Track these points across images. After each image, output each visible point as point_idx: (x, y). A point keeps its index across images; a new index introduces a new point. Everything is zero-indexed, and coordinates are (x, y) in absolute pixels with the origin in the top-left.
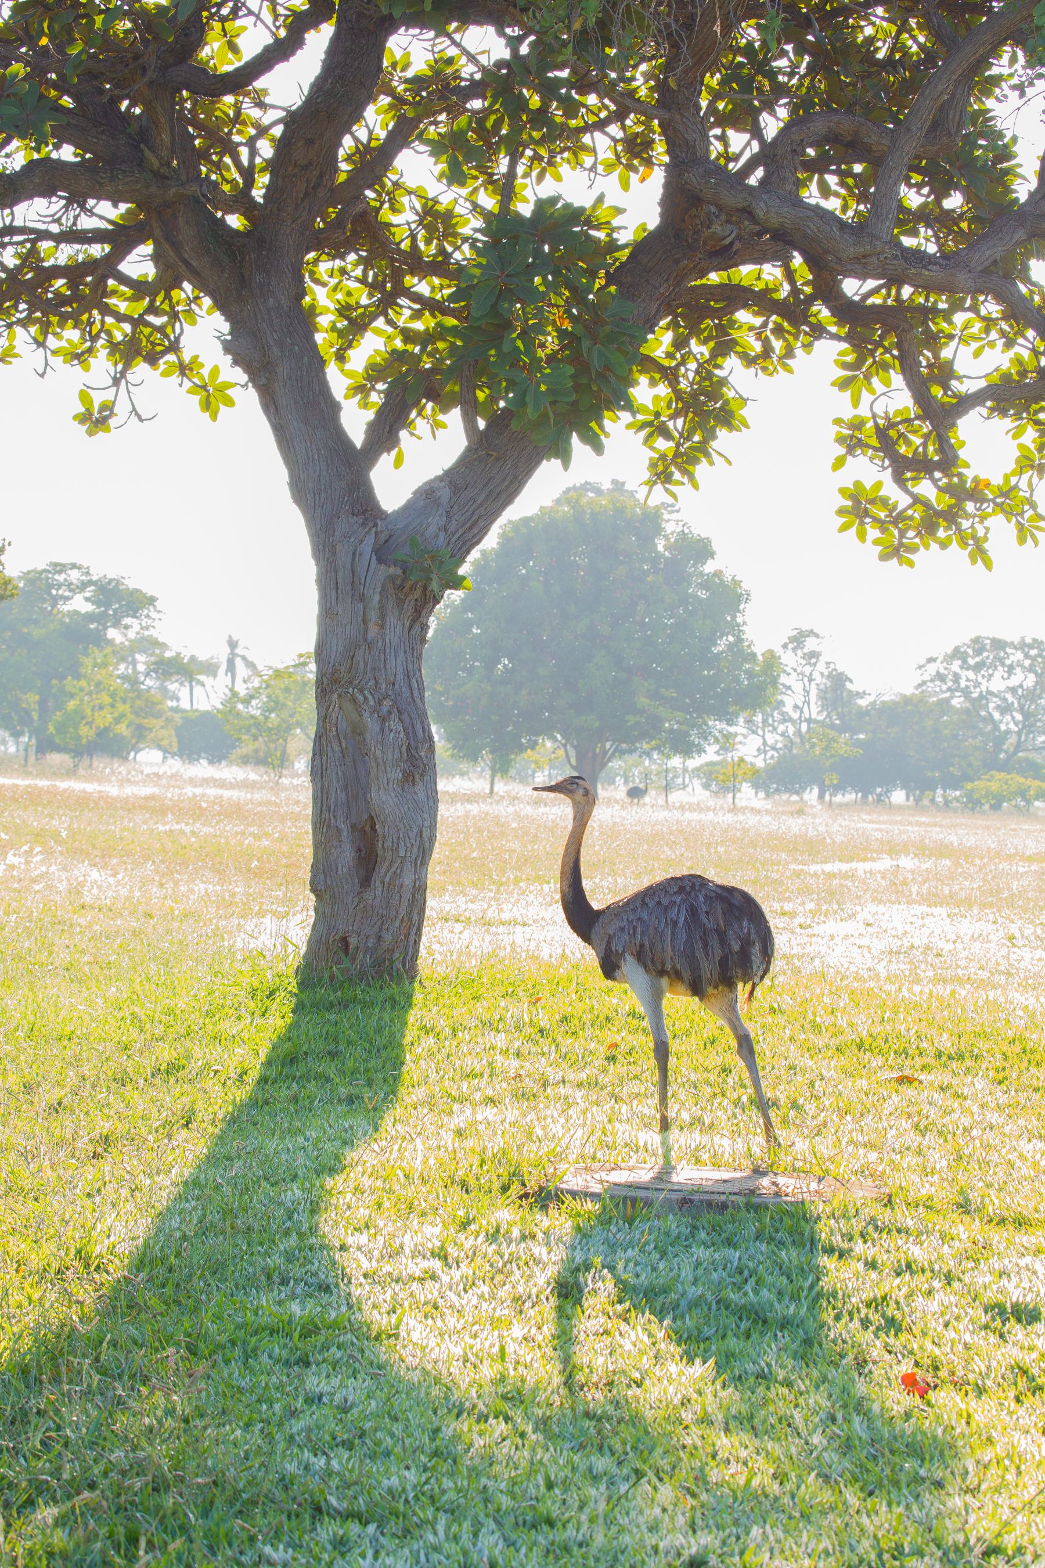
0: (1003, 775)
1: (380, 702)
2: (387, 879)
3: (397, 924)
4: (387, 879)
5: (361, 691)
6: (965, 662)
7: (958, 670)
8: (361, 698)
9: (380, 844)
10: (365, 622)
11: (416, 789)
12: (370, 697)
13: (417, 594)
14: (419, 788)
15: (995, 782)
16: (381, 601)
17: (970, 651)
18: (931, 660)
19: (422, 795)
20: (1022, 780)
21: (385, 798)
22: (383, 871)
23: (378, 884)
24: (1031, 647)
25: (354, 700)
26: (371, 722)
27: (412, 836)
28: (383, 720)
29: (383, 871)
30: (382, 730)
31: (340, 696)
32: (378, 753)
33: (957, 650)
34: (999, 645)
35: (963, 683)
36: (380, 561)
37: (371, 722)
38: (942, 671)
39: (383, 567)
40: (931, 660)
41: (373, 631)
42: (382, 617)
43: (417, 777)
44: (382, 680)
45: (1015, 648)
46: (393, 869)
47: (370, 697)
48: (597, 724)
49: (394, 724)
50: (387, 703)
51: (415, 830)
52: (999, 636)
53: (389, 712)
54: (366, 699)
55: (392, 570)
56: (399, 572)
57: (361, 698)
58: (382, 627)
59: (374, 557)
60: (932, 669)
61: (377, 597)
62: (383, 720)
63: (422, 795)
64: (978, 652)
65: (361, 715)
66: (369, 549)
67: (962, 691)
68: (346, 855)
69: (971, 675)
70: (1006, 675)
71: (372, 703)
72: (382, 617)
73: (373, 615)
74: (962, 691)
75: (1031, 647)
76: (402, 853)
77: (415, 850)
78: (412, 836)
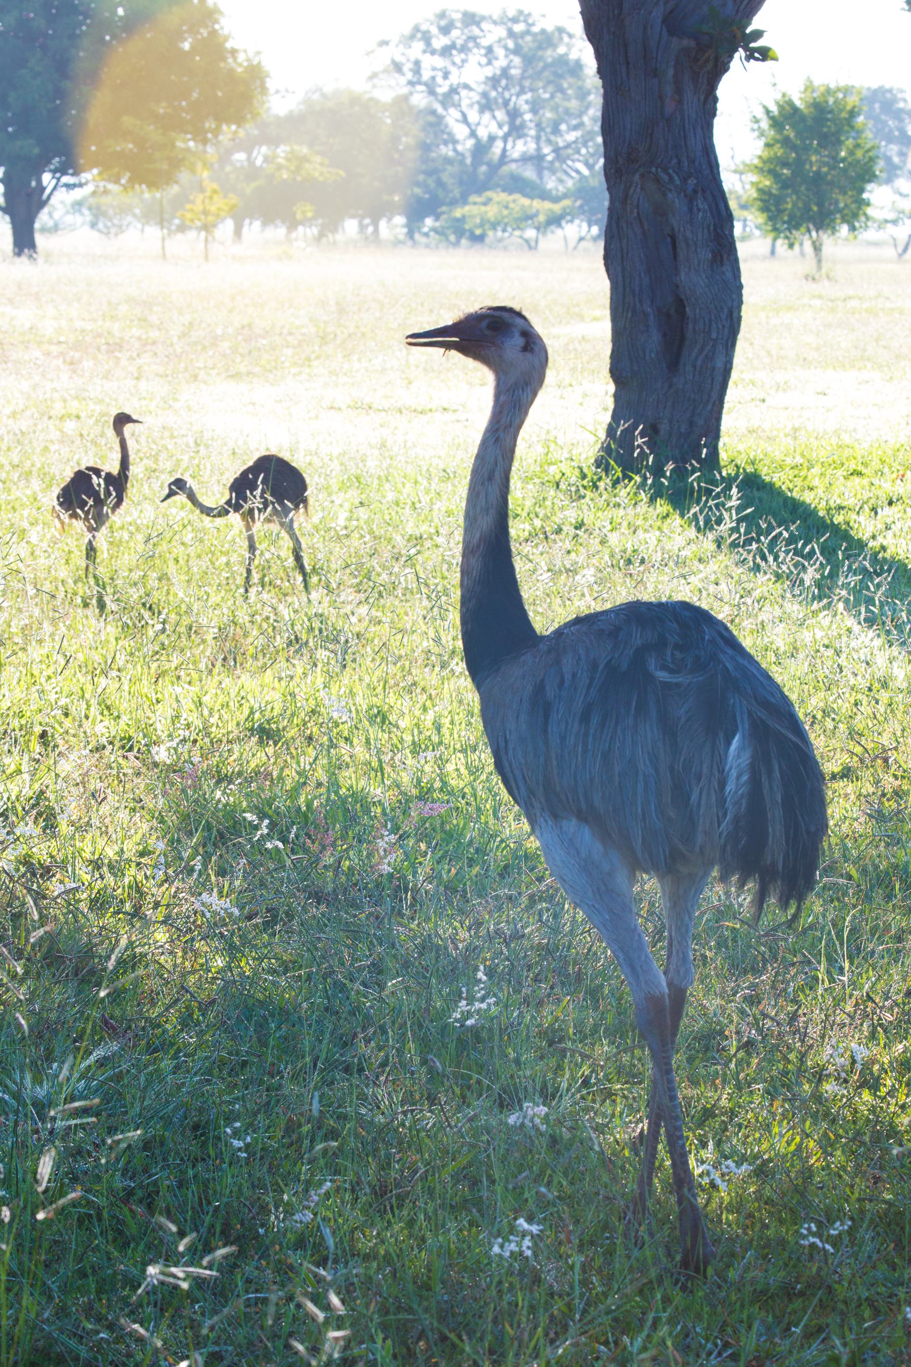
0: (503, 197)
1: (684, 180)
2: (699, 363)
3: (709, 408)
4: (699, 363)
5: (665, 170)
6: (428, 43)
7: (420, 57)
8: (665, 177)
9: (690, 326)
10: (660, 98)
11: (724, 268)
12: (675, 177)
13: (710, 66)
14: (727, 268)
15: (495, 204)
16: (675, 75)
17: (434, 30)
18: (384, 43)
19: (729, 275)
20: (526, 202)
21: (693, 279)
22: (694, 354)
23: (689, 368)
24: (515, 20)
25: (658, 180)
26: (678, 203)
27: (723, 316)
28: (691, 200)
29: (694, 354)
30: (690, 210)
31: (642, 176)
32: (688, 233)
33: (417, 29)
34: (471, 19)
35: (426, 75)
36: (671, 33)
37: (678, 203)
38: (399, 58)
39: (675, 40)
40: (384, 43)
41: (670, 106)
42: (679, 91)
43: (725, 257)
44: (684, 159)
45: (495, 23)
46: (705, 353)
47: (675, 177)
48: (36, 151)
49: (701, 203)
50: (692, 182)
51: (726, 311)
52: (471, 9)
53: (695, 192)
54: (671, 179)
55: (685, 42)
56: (693, 44)
57: (665, 177)
58: (680, 102)
59: (664, 29)
60: (383, 58)
61: (671, 72)
62: (691, 200)
63: (729, 275)
64: (445, 30)
65: (664, 195)
66: (659, 21)
67: (426, 84)
68: (653, 340)
69: (439, 61)
70: (484, 61)
71: (678, 182)
72: (679, 91)
73: (669, 90)
74: (426, 84)
75: (515, 20)
76: (714, 336)
77: (726, 331)
78: (723, 316)
